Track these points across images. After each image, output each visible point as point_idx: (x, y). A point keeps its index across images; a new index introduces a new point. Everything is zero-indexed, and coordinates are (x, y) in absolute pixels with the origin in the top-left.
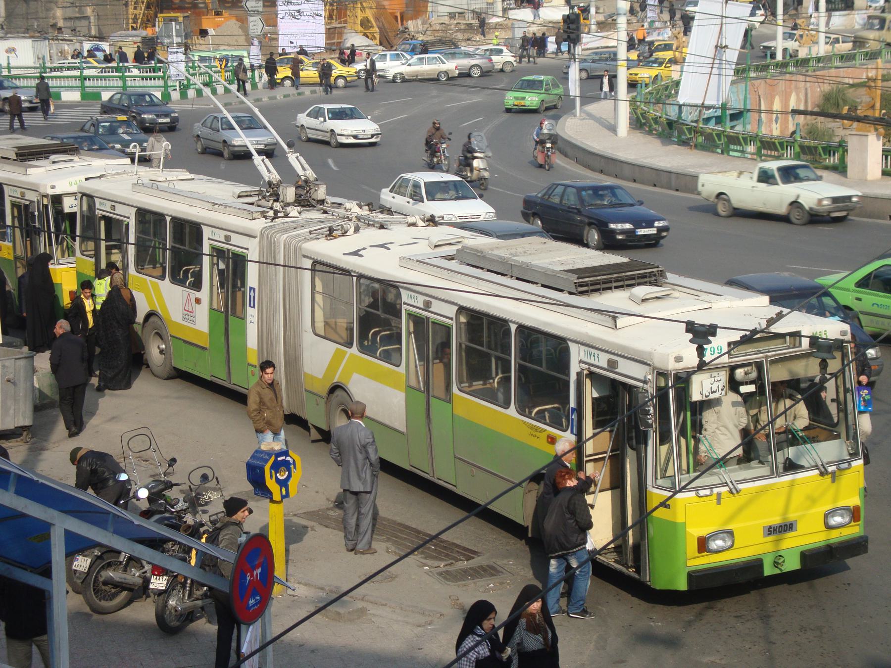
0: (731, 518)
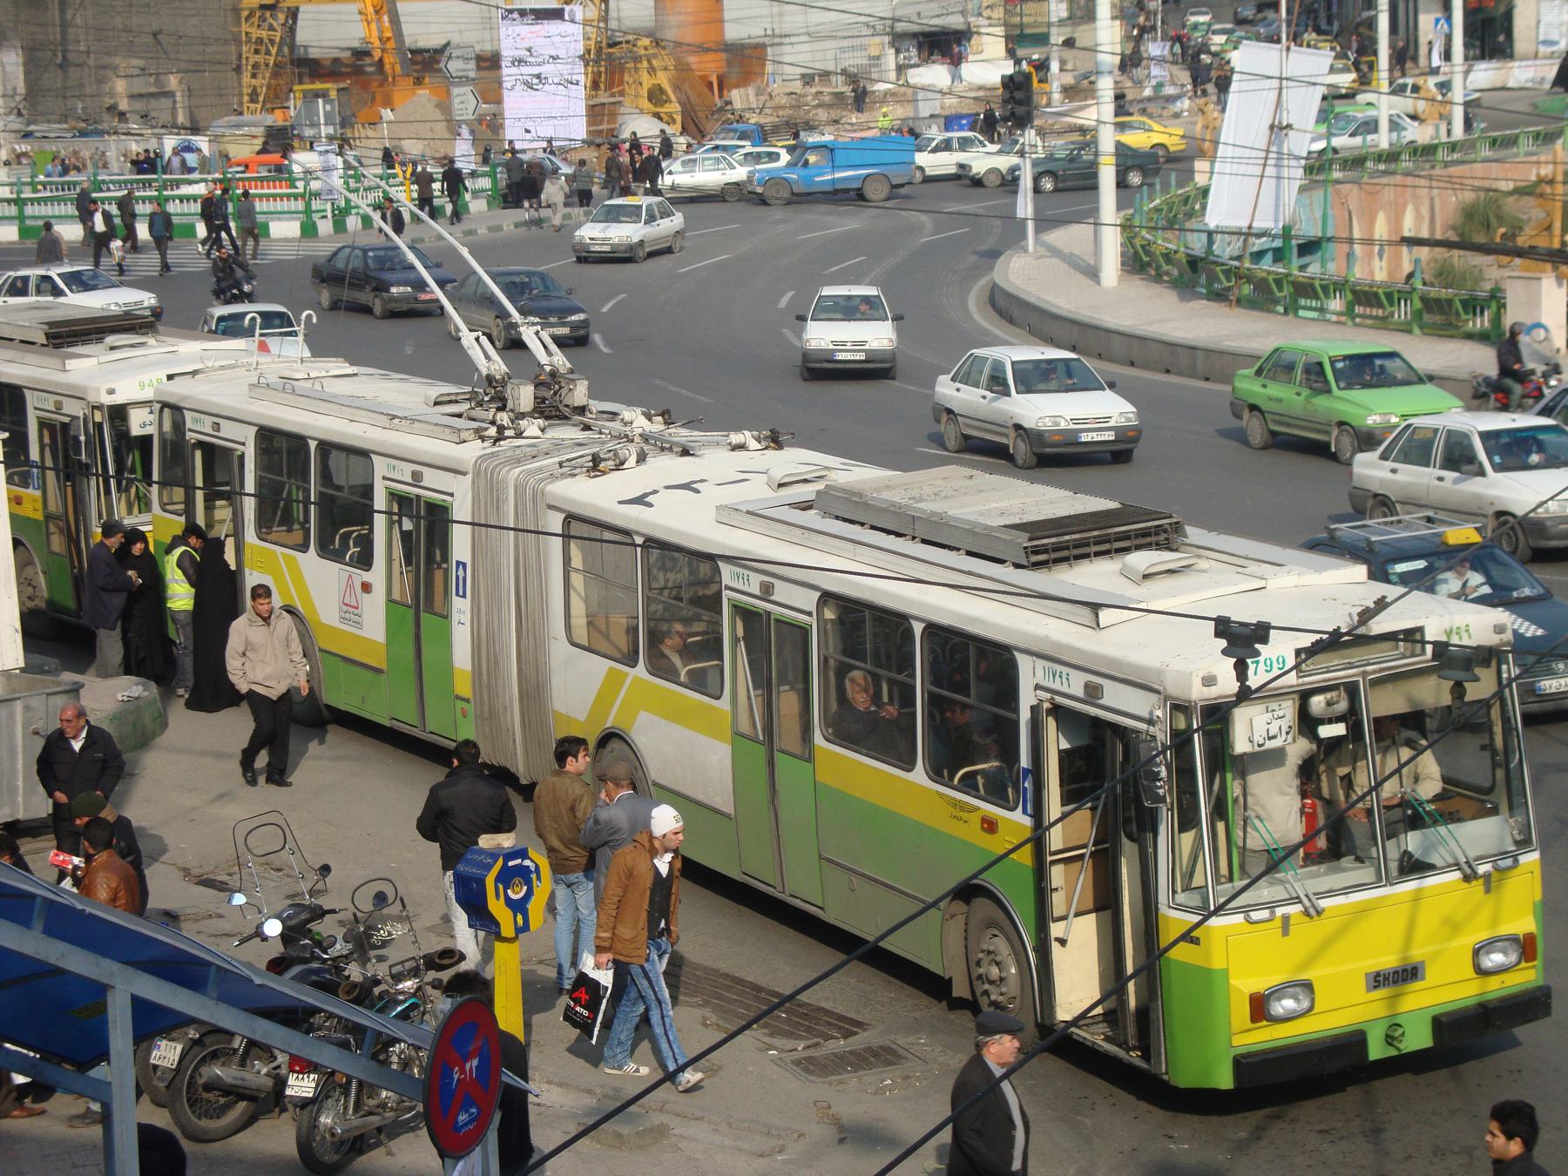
0: (1312, 959)
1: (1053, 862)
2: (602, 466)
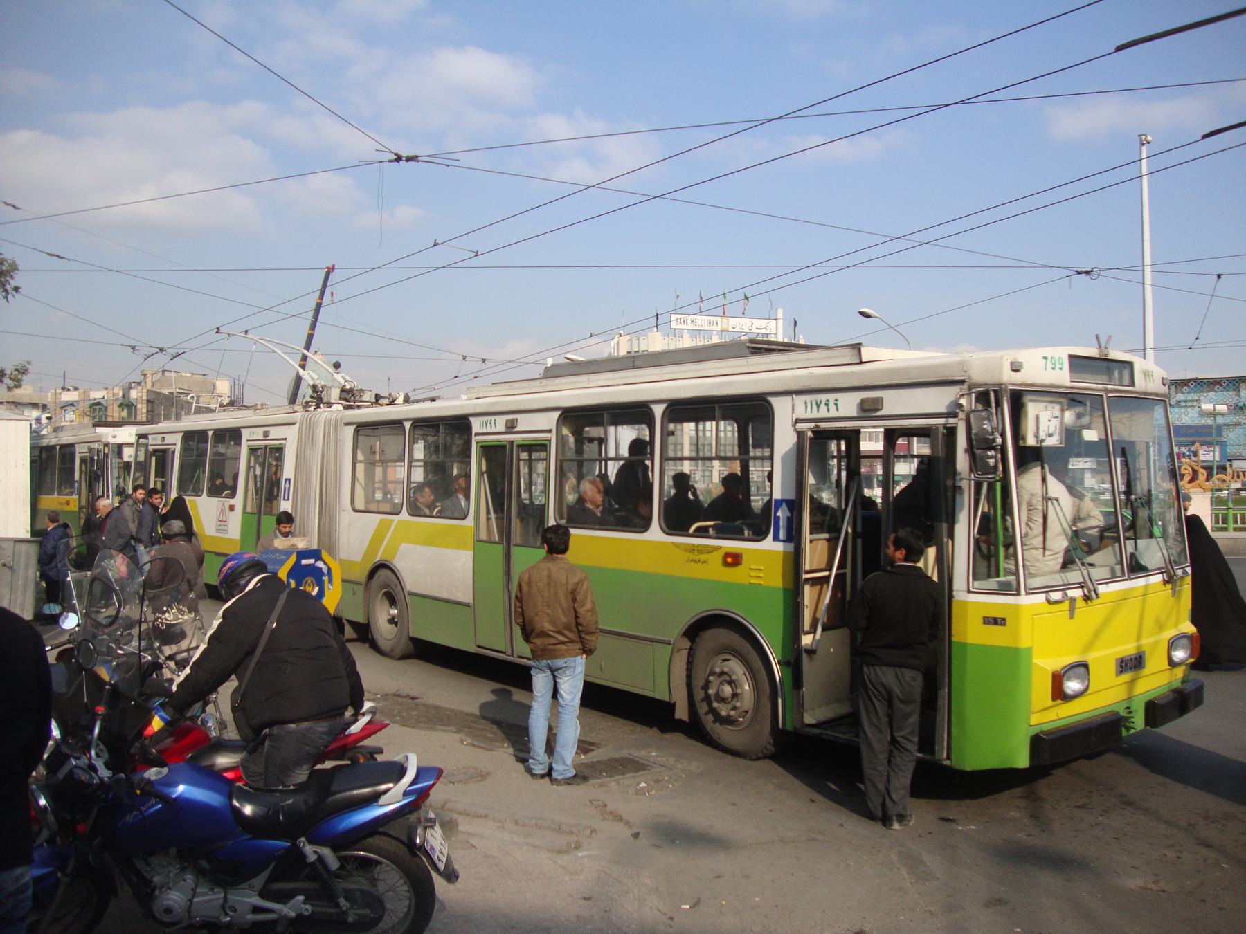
0: (1089, 646)
1: (807, 580)
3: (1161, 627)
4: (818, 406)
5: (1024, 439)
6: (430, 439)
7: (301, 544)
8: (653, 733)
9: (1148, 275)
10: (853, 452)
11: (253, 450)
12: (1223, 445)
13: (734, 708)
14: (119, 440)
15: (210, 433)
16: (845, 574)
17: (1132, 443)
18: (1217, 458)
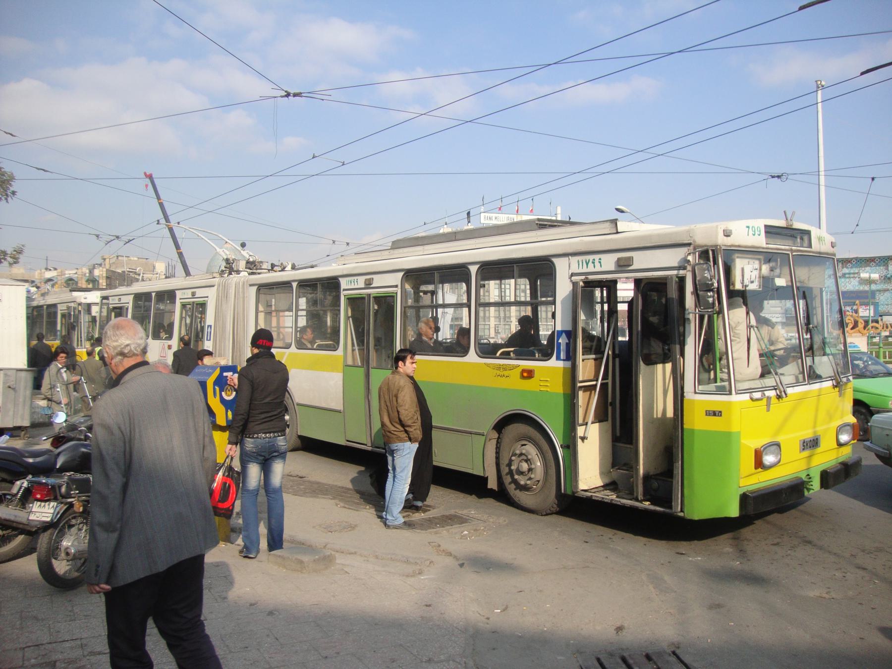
0: (778, 431)
1: (581, 387)
2: (275, 268)
3: (830, 417)
4: (587, 264)
5: (734, 285)
6: (310, 296)
7: (223, 363)
8: (472, 499)
9: (822, 179)
10: (612, 299)
11: (184, 306)
12: (876, 305)
13: (530, 479)
14: (88, 301)
15: (154, 294)
16: (607, 383)
17: (811, 289)
18: (872, 314)
